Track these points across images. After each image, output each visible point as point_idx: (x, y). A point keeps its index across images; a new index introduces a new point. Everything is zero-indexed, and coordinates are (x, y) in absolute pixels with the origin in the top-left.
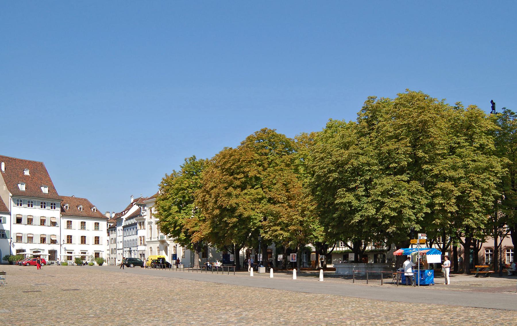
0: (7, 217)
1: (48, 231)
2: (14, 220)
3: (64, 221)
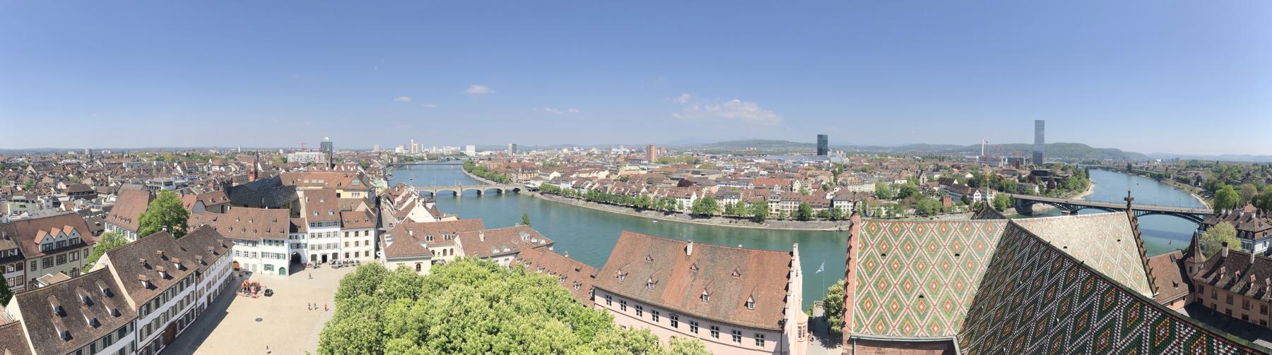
1: (332, 240)
2: (309, 235)
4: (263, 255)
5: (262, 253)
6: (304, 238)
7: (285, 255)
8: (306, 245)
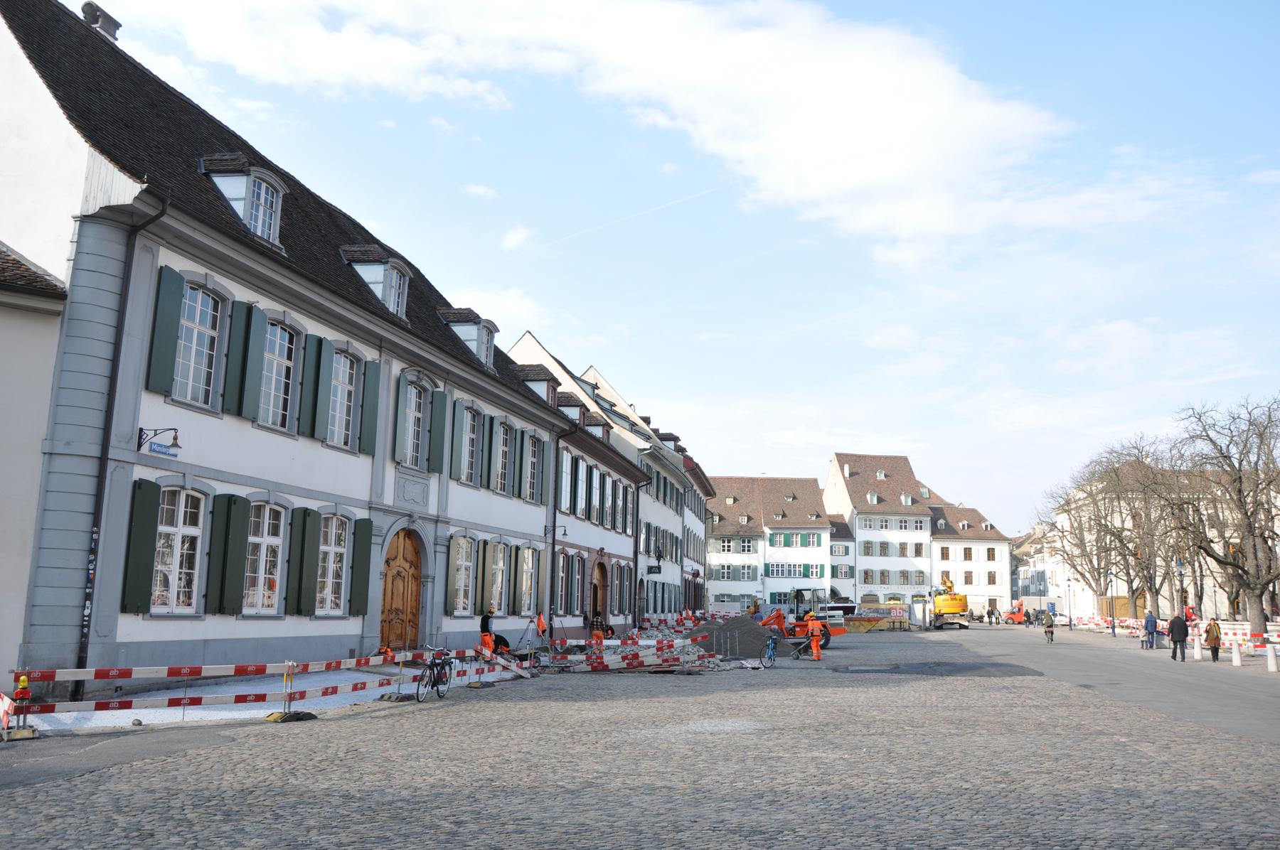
0: (850, 544)
3: (937, 547)
4: (768, 571)
5: (766, 566)
6: (847, 553)
7: (822, 566)
8: (852, 569)
